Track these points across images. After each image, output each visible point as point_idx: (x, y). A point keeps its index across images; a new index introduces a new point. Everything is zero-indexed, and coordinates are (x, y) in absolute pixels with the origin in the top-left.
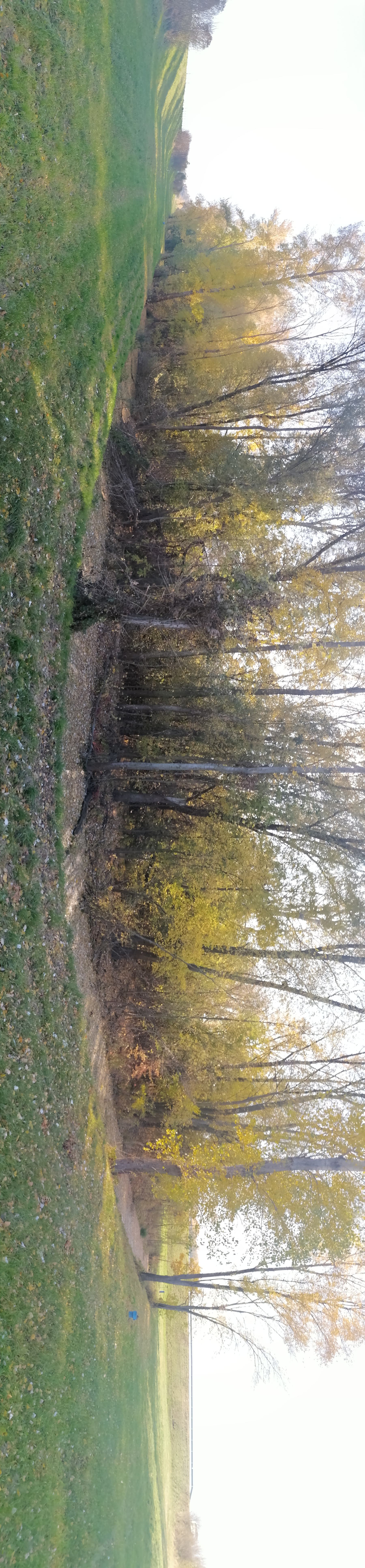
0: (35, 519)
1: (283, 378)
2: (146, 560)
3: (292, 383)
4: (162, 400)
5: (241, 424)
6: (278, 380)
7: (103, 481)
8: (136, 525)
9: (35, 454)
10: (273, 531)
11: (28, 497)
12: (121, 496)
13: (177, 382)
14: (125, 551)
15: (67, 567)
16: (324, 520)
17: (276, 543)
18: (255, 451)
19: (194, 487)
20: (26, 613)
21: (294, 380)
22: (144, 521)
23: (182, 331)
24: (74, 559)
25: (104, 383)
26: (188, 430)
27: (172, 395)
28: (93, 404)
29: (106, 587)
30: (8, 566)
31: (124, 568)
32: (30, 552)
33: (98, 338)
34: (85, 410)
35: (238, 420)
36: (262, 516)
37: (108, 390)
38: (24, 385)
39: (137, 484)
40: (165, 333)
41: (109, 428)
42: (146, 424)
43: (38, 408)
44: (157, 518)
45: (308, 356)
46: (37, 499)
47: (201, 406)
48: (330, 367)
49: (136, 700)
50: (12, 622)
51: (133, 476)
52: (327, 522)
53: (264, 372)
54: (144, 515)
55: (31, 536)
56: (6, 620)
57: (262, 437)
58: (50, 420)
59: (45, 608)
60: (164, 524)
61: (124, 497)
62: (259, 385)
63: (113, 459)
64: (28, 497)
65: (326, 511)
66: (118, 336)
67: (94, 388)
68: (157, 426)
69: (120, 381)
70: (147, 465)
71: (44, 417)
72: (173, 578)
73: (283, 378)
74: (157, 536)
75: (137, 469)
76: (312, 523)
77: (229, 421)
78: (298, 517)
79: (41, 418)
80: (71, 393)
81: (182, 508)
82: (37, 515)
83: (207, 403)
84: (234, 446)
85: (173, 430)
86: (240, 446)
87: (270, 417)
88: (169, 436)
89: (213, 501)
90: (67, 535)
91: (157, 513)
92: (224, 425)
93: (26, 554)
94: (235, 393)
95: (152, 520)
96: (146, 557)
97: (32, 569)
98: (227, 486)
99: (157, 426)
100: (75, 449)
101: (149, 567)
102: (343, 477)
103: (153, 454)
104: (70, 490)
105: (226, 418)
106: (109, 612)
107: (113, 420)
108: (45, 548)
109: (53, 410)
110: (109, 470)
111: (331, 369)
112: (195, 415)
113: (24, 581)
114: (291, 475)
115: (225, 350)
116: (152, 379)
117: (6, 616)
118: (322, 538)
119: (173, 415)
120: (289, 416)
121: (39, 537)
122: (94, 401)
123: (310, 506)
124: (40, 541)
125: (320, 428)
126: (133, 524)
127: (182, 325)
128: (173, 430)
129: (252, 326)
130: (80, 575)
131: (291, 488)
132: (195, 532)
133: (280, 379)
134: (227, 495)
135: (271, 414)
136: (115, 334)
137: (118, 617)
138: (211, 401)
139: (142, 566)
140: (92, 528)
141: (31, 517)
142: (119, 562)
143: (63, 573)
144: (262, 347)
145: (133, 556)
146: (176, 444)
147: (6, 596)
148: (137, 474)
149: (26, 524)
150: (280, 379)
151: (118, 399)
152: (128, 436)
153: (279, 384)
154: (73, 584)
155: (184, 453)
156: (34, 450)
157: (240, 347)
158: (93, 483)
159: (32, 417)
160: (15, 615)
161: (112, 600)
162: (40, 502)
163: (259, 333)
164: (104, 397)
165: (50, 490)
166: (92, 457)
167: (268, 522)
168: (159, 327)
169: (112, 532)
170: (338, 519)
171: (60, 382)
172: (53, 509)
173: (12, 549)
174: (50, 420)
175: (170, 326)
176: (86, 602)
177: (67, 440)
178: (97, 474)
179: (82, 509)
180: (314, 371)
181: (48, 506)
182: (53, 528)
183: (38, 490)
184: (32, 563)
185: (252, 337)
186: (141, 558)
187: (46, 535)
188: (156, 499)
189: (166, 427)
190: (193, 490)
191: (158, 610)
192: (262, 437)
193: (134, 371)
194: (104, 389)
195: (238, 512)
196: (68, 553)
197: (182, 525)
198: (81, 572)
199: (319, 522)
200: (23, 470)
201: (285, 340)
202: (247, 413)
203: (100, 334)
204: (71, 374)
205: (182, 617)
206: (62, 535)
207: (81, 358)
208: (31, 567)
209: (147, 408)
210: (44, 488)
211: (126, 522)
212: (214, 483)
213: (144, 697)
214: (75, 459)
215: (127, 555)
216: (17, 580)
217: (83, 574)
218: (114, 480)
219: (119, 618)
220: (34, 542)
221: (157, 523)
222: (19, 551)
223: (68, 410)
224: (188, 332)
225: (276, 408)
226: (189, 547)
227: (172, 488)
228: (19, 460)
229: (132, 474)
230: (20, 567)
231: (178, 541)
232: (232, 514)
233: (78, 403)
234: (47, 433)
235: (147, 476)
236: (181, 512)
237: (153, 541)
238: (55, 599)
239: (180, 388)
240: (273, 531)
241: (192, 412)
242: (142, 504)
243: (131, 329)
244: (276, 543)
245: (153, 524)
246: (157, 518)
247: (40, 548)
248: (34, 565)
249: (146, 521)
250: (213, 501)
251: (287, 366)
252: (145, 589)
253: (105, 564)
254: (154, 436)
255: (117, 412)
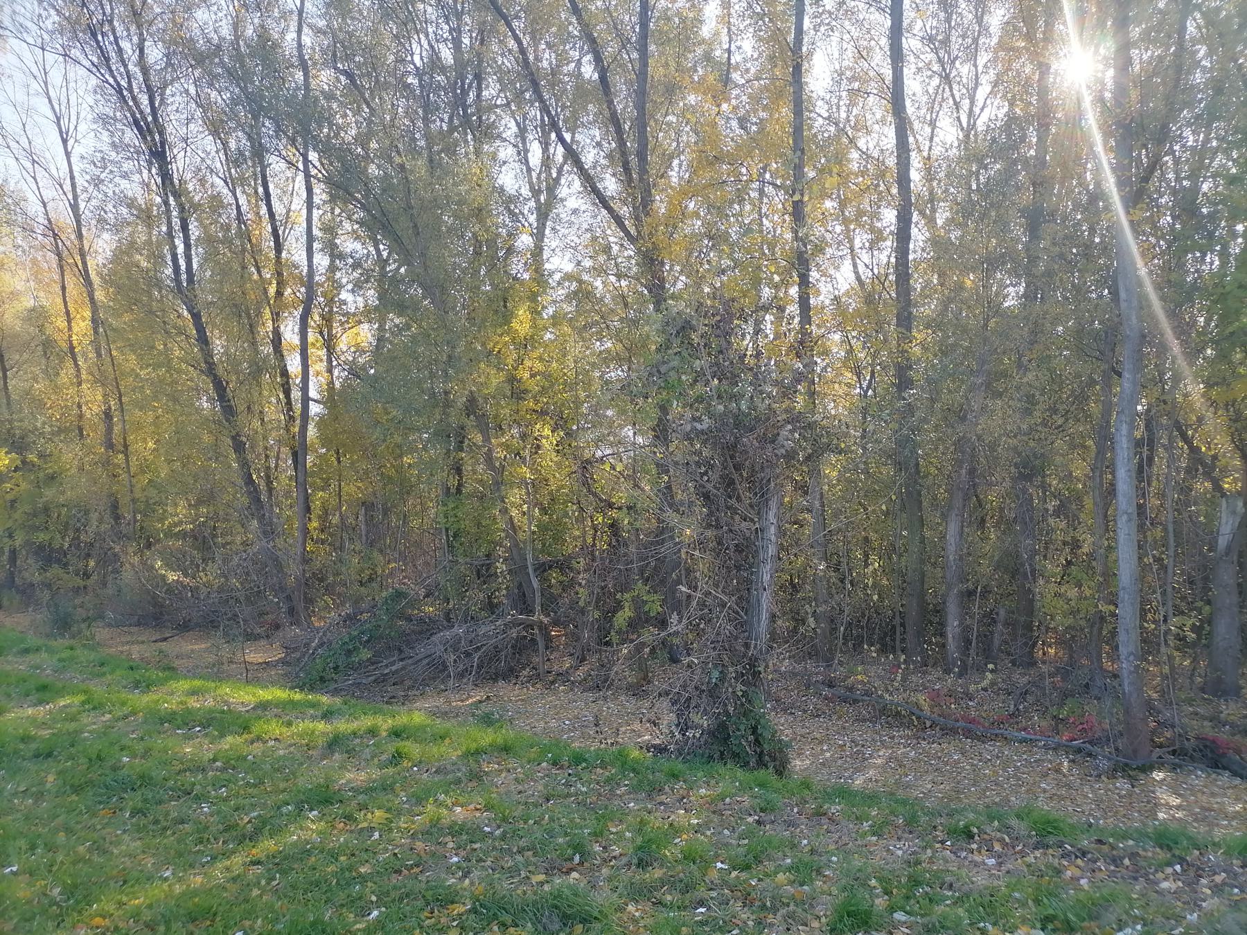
0: (527, 863)
1: (181, 249)
2: (626, 596)
3: (195, 231)
4: (226, 560)
5: (294, 365)
6: (183, 267)
7: (439, 702)
8: (546, 620)
9: (360, 875)
10: (556, 299)
11: (472, 883)
12: (476, 656)
13: (180, 523)
14: (608, 644)
15: (640, 781)
16: (530, 183)
17: (583, 294)
18: (365, 334)
19: (453, 482)
20: (744, 875)
21: (185, 228)
22: (538, 600)
23: (46, 510)
24: (624, 764)
25: (174, 713)
26: (307, 498)
27: (214, 536)
28: (229, 739)
29: (684, 687)
30: (635, 921)
31: (643, 644)
32: (605, 871)
33: (33, 746)
34: (245, 758)
35: (285, 373)
36: (522, 322)
37: (194, 703)
38: (168, 923)
39: (449, 620)
40: (48, 556)
41: (298, 696)
42: (289, 598)
43: (234, 879)
44: (530, 570)
45: (124, 184)
46: (480, 860)
47: (245, 464)
48: (157, 137)
49: (933, 617)
50: (763, 907)
51: (427, 628)
52: (534, 175)
53: (161, 301)
54: (523, 602)
55: (568, 873)
56: (759, 923)
57: (328, 319)
58: (268, 845)
59: (734, 830)
60: (542, 551)
61: (478, 648)
62: (196, 317)
63: (382, 680)
64: (472, 885)
65: (509, 179)
66: (43, 688)
67: (188, 738)
68: (294, 570)
69: (171, 671)
70: (399, 595)
71: (258, 863)
72: (663, 532)
73: (181, 249)
74: (571, 569)
75: (409, 619)
76: (538, 209)
77: (287, 393)
78: (525, 241)
79: (259, 870)
80: (198, 798)
81: (505, 511)
82: (519, 858)
83: (239, 447)
84: (350, 386)
85: (305, 531)
86: (355, 371)
87: (279, 294)
88: (323, 542)
89: (487, 439)
90: (568, 785)
91: (518, 570)
92: (298, 407)
93: (610, 879)
94: (215, 376)
95: (535, 583)
96: (619, 596)
97: (642, 864)
98: (448, 404)
99: (294, 570)
100: (349, 776)
101: (640, 588)
102: (428, 136)
103: (371, 580)
104: (458, 782)
105: (279, 400)
106: (743, 683)
107: (273, 684)
108: (596, 835)
109: (242, 839)
110: (411, 688)
111: (161, 133)
112: (268, 476)
113: (670, 882)
114: (423, 255)
115: (105, 395)
116: (170, 589)
117: (751, 923)
118: (571, 191)
119: (269, 531)
120: (279, 248)
121: (570, 851)
122: (222, 736)
123: (497, 209)
124: (579, 848)
125: (308, 176)
126: (544, 629)
127: (27, 508)
128: (305, 531)
129: (37, 316)
130: (660, 750)
131: (456, 254)
132: (560, 478)
133: (182, 263)
134: (472, 406)
135: (272, 290)
136: (33, 698)
137: (753, 663)
138: (233, 438)
139: (638, 603)
140: (553, 724)
141: (523, 874)
142: (629, 657)
143: (654, 790)
144: (99, 295)
145: (617, 627)
146: (343, 525)
147: (702, 923)
148: (421, 621)
149: (542, 884)
150: (182, 263)
151: (218, 673)
152: (321, 645)
153: (195, 266)
154: (679, 766)
155: (368, 506)
156: (348, 877)
157: (99, 355)
158: (440, 725)
159: (256, 892)
160: (747, 901)
161: (716, 674)
162: (486, 853)
163: (59, 300)
164: (211, 711)
165: (455, 830)
166: (372, 732)
167: (536, 312)
168: (31, 572)
169: (563, 676)
170: (526, 151)
171: (165, 829)
172: (504, 819)
173: (596, 914)
174: (268, 845)
175: (28, 543)
176: (720, 735)
177: (324, 798)
178: (418, 718)
179: (506, 749)
180: (166, 176)
181: (498, 832)
182: (552, 820)
183: (455, 859)
184: (629, 865)
185: (69, 322)
186: (622, 608)
187: (566, 834)
188: (484, 572)
189: (299, 550)
190: (460, 485)
191: (738, 568)
192: (328, 319)
193: (148, 634)
194: (189, 711)
195: (512, 379)
196: (608, 781)
197: (544, 511)
198: (654, 746)
199: (536, 193)
200: (401, 899)
201: (80, 236)
202: (267, 349)
203: (25, 739)
204: (145, 801)
205: (752, 514)
206: (568, 795)
207: (90, 783)
208: (638, 866)
209: (247, 598)
210: (451, 845)
211: (541, 645)
212: (442, 434)
213: (923, 605)
214: (376, 774)
215: (615, 638)
216: (669, 898)
217: (657, 742)
218: (437, 673)
219: (756, 659)
220: (581, 863)
221: (542, 569)
222: (603, 898)
223: (241, 801)
224: (49, 493)
225: (256, 277)
226: (595, 495)
227: (455, 536)
228: (375, 913)
229: (421, 633)
230: (638, 893)
231: (580, 520)
232: (517, 392)
233: (226, 776)
234: (304, 852)
235: (427, 596)
236: (514, 512)
237: (582, 578)
238: (713, 808)
239: (198, 516)
240: (556, 299)
241: (263, 486)
242: (497, 606)
243: (26, 651)
244: (583, 294)
245: (544, 580)
246: (530, 570)
247: (597, 848)
248: (635, 861)
249: (538, 595)
250: (487, 439)
251: (149, 242)
252: (689, 596)
253: (637, 690)
254: (321, 580)
255: (253, 675)
